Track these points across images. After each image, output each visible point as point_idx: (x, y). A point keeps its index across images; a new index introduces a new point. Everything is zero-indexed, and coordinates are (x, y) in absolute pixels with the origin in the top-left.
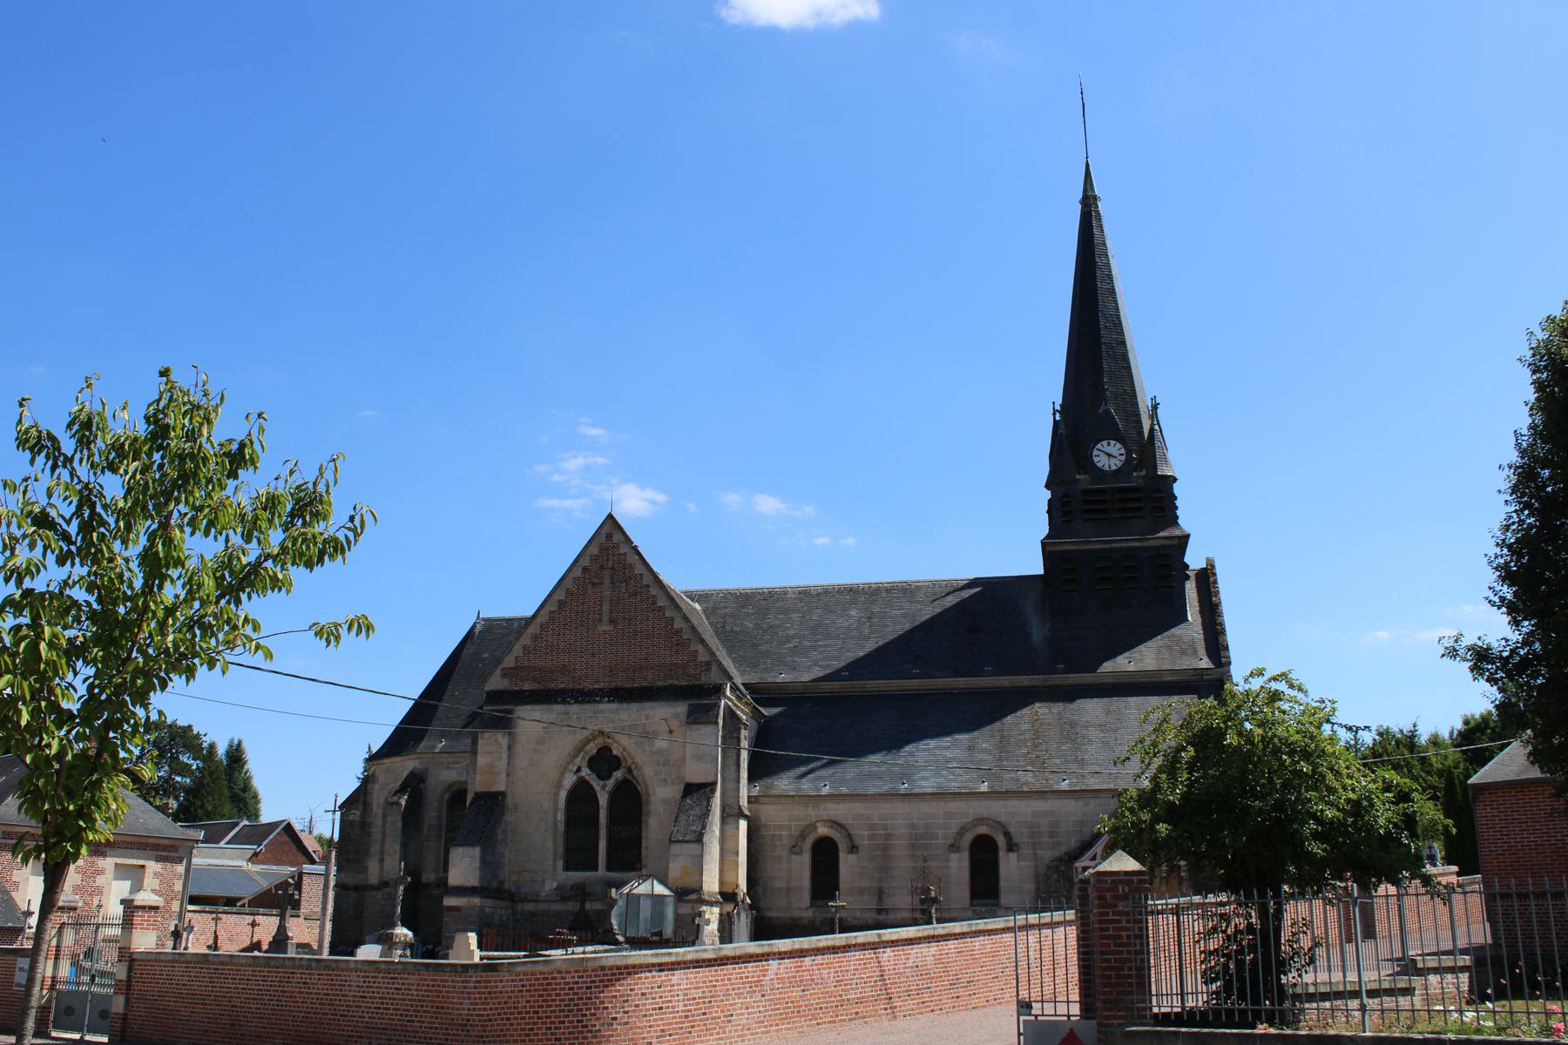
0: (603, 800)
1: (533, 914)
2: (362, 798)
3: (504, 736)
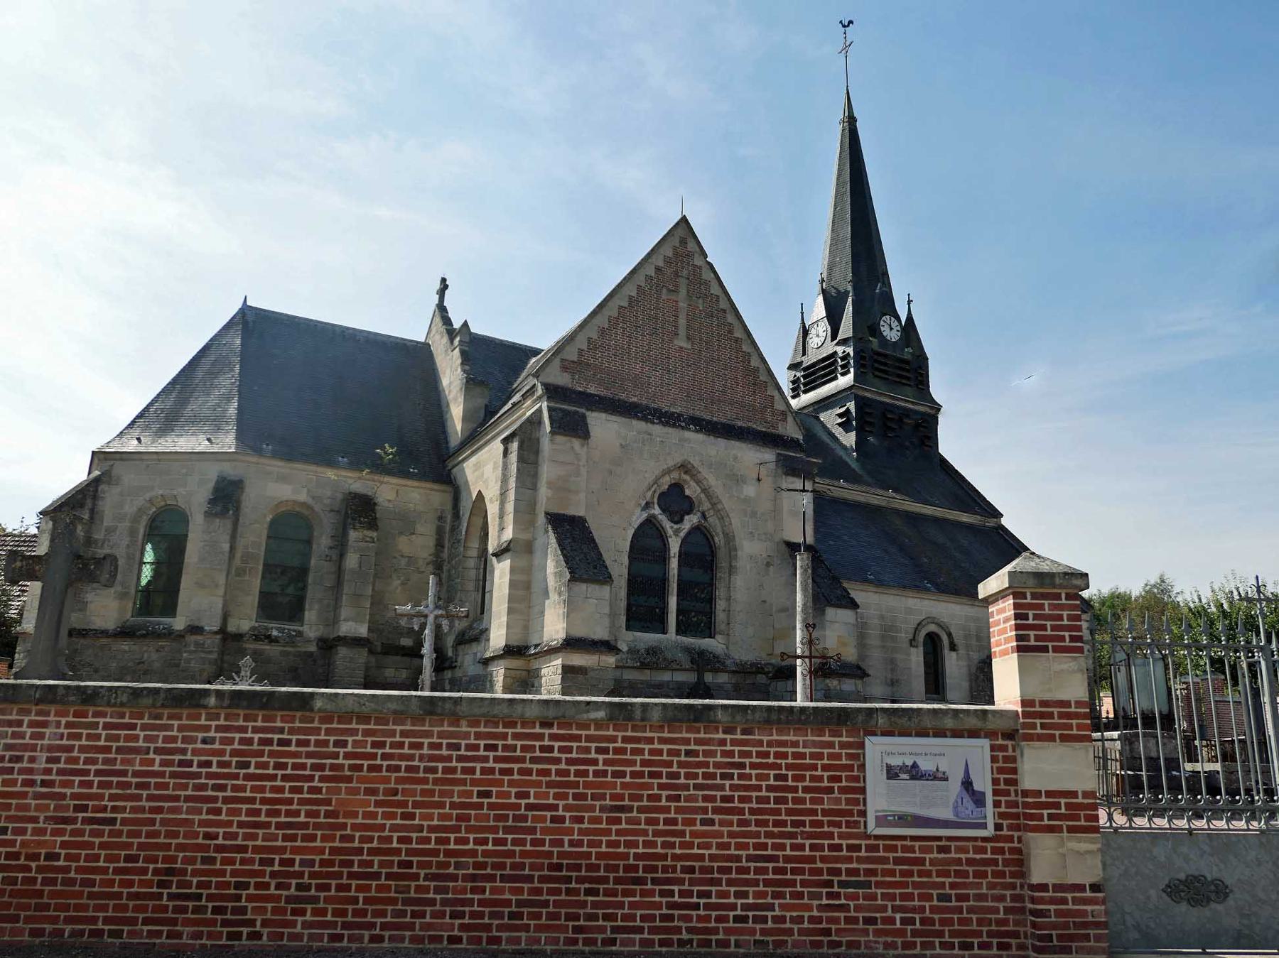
0: (675, 546)
2: (89, 503)
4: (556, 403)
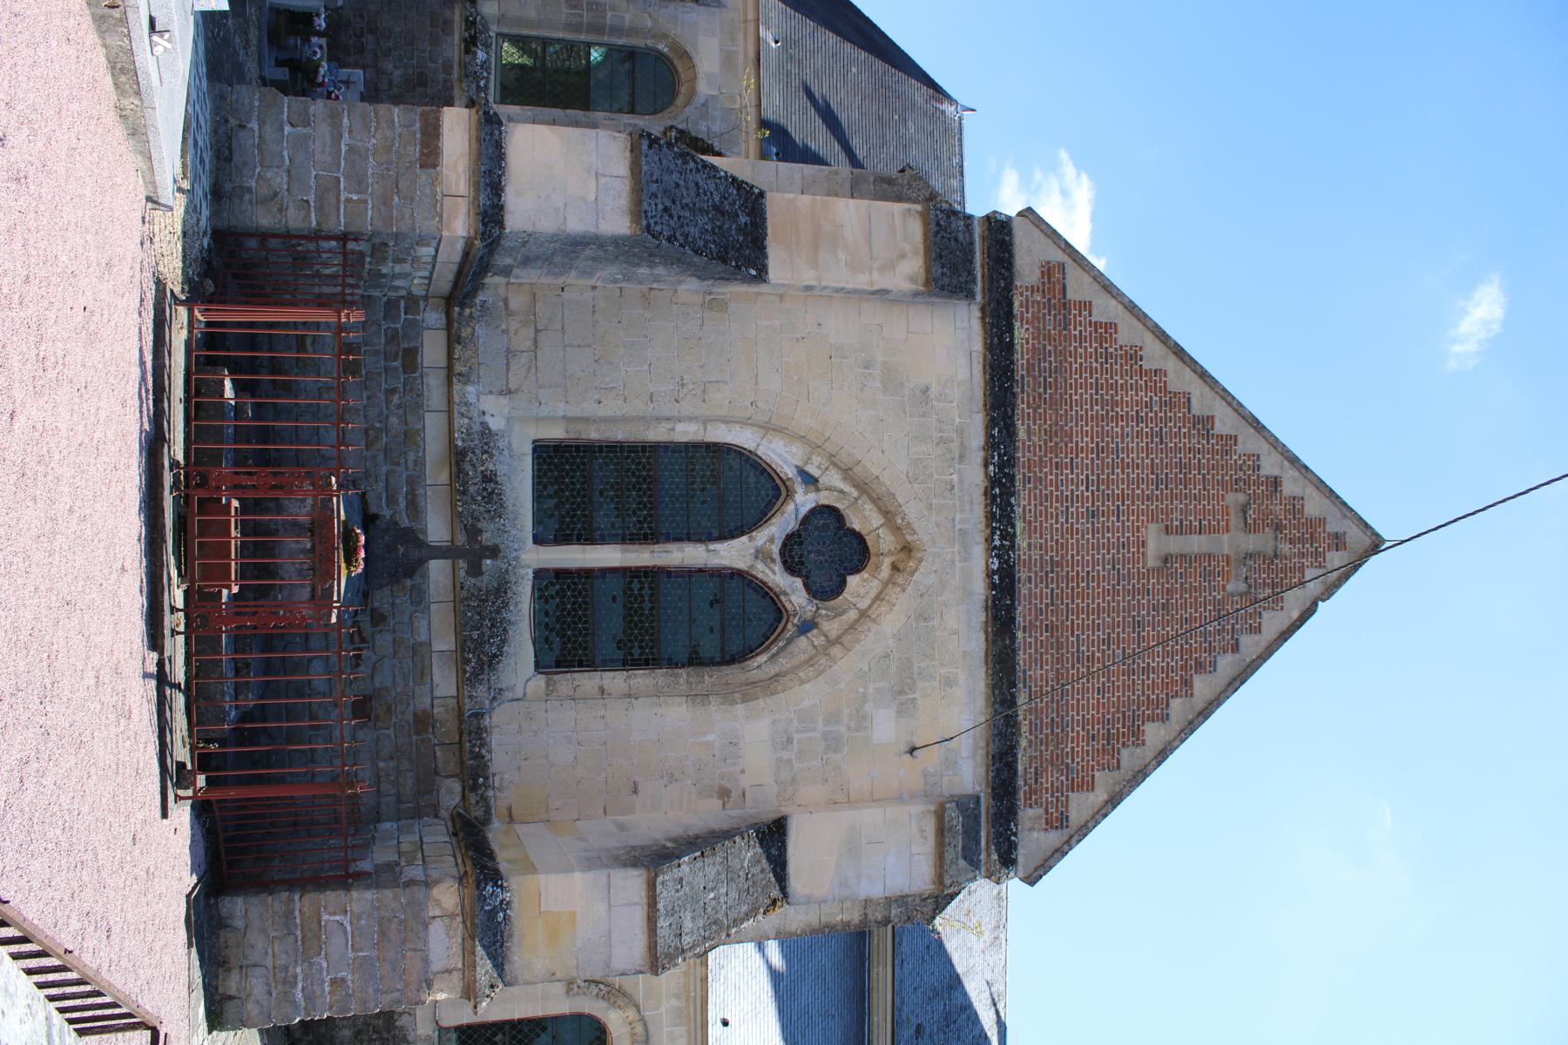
0: (731, 554)
1: (411, 358)
3: (913, 280)
4: (983, 239)
